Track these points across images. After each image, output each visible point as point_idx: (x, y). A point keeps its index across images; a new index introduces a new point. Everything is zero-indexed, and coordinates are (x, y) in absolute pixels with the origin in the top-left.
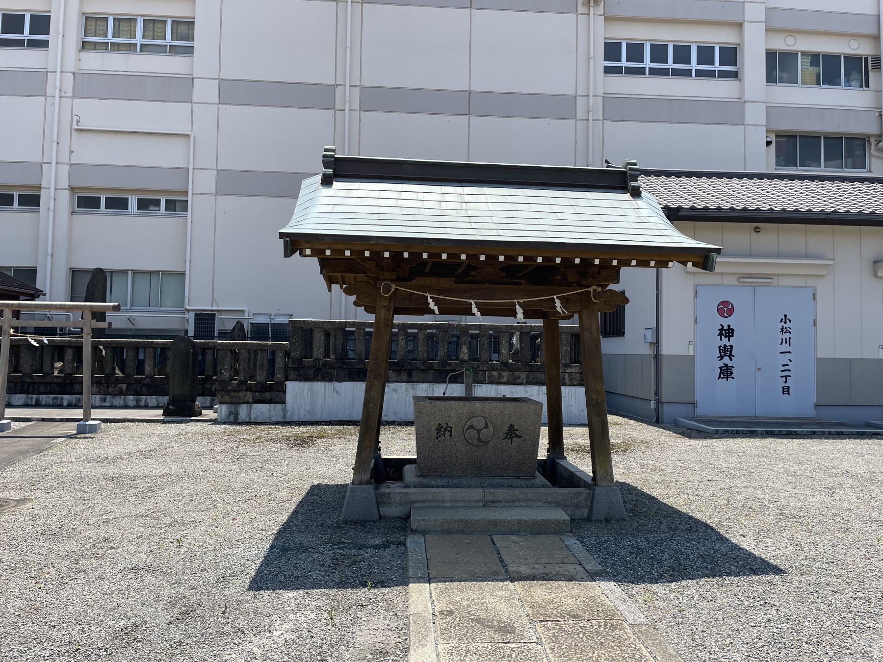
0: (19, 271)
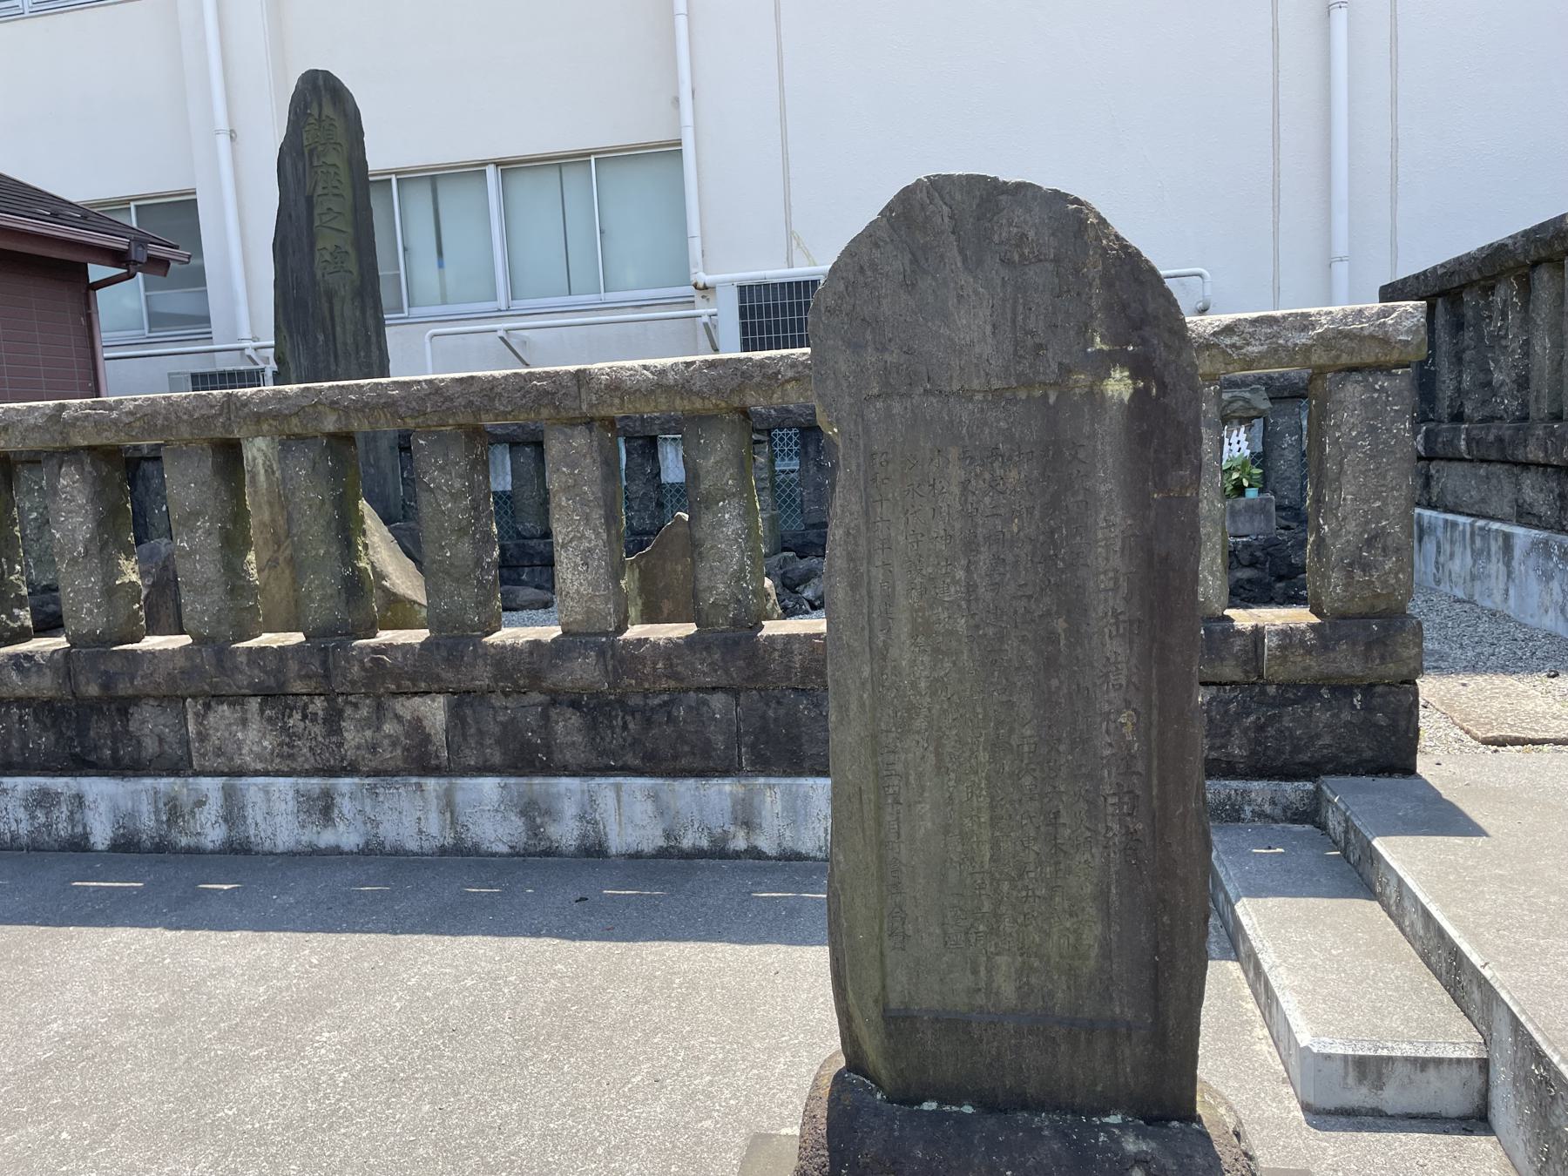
0: (151, 208)
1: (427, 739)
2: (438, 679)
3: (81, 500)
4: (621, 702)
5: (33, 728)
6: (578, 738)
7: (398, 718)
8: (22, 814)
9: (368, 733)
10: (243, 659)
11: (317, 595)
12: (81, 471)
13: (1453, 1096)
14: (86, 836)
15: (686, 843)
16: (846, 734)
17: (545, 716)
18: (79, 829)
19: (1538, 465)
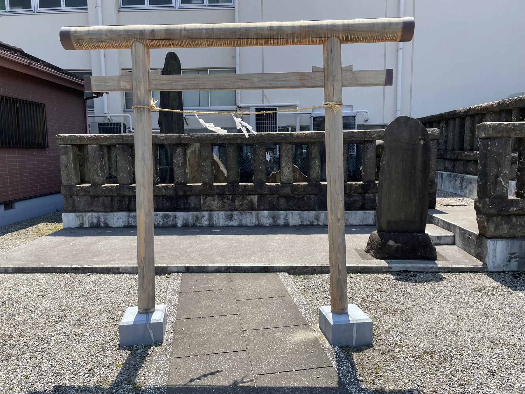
1: (253, 204)
2: (257, 191)
3: (181, 154)
4: (293, 197)
5: (165, 201)
6: (284, 203)
7: (248, 200)
8: (161, 220)
9: (241, 203)
10: (215, 187)
11: (232, 175)
12: (182, 148)
13: (450, 241)
14: (176, 224)
15: (305, 223)
16: (153, 269)
17: (278, 199)
18: (175, 223)
19: (449, 159)
